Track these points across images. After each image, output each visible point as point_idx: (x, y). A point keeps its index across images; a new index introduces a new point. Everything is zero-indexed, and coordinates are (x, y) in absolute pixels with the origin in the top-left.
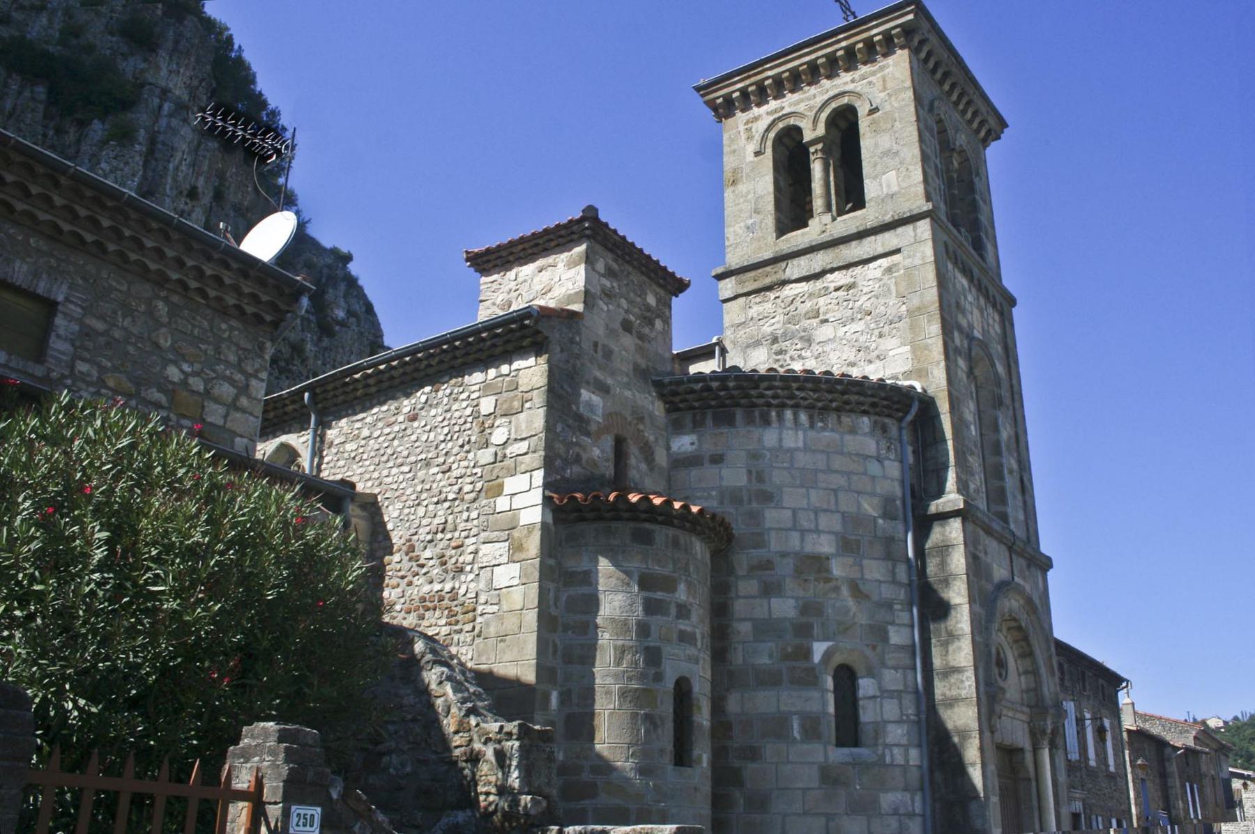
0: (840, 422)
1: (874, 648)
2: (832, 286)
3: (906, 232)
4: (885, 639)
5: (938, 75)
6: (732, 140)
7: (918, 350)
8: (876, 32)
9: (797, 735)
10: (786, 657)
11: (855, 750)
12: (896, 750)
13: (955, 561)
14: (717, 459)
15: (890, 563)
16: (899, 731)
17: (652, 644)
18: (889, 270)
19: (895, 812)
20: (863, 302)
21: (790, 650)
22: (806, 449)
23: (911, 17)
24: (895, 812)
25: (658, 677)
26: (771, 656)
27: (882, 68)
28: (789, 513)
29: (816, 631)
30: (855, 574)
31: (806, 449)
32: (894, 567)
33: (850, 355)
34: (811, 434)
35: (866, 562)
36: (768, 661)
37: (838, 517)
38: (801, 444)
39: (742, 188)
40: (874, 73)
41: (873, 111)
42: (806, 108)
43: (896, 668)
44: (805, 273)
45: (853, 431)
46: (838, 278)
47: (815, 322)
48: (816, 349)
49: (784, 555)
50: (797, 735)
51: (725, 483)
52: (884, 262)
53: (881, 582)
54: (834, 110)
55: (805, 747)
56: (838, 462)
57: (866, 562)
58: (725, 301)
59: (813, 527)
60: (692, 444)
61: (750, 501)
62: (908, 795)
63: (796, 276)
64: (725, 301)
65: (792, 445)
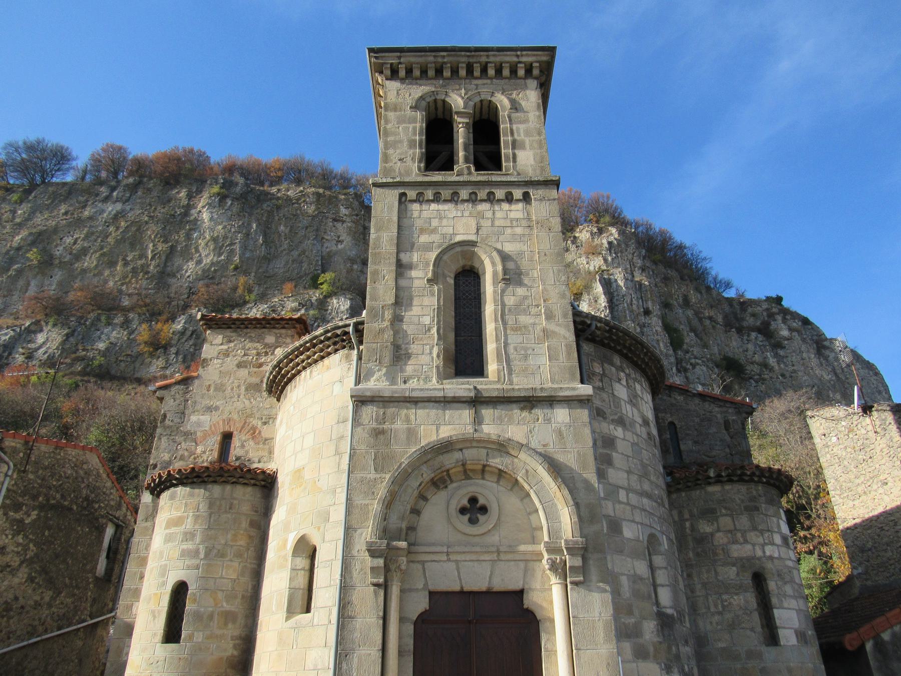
45: (328, 368)
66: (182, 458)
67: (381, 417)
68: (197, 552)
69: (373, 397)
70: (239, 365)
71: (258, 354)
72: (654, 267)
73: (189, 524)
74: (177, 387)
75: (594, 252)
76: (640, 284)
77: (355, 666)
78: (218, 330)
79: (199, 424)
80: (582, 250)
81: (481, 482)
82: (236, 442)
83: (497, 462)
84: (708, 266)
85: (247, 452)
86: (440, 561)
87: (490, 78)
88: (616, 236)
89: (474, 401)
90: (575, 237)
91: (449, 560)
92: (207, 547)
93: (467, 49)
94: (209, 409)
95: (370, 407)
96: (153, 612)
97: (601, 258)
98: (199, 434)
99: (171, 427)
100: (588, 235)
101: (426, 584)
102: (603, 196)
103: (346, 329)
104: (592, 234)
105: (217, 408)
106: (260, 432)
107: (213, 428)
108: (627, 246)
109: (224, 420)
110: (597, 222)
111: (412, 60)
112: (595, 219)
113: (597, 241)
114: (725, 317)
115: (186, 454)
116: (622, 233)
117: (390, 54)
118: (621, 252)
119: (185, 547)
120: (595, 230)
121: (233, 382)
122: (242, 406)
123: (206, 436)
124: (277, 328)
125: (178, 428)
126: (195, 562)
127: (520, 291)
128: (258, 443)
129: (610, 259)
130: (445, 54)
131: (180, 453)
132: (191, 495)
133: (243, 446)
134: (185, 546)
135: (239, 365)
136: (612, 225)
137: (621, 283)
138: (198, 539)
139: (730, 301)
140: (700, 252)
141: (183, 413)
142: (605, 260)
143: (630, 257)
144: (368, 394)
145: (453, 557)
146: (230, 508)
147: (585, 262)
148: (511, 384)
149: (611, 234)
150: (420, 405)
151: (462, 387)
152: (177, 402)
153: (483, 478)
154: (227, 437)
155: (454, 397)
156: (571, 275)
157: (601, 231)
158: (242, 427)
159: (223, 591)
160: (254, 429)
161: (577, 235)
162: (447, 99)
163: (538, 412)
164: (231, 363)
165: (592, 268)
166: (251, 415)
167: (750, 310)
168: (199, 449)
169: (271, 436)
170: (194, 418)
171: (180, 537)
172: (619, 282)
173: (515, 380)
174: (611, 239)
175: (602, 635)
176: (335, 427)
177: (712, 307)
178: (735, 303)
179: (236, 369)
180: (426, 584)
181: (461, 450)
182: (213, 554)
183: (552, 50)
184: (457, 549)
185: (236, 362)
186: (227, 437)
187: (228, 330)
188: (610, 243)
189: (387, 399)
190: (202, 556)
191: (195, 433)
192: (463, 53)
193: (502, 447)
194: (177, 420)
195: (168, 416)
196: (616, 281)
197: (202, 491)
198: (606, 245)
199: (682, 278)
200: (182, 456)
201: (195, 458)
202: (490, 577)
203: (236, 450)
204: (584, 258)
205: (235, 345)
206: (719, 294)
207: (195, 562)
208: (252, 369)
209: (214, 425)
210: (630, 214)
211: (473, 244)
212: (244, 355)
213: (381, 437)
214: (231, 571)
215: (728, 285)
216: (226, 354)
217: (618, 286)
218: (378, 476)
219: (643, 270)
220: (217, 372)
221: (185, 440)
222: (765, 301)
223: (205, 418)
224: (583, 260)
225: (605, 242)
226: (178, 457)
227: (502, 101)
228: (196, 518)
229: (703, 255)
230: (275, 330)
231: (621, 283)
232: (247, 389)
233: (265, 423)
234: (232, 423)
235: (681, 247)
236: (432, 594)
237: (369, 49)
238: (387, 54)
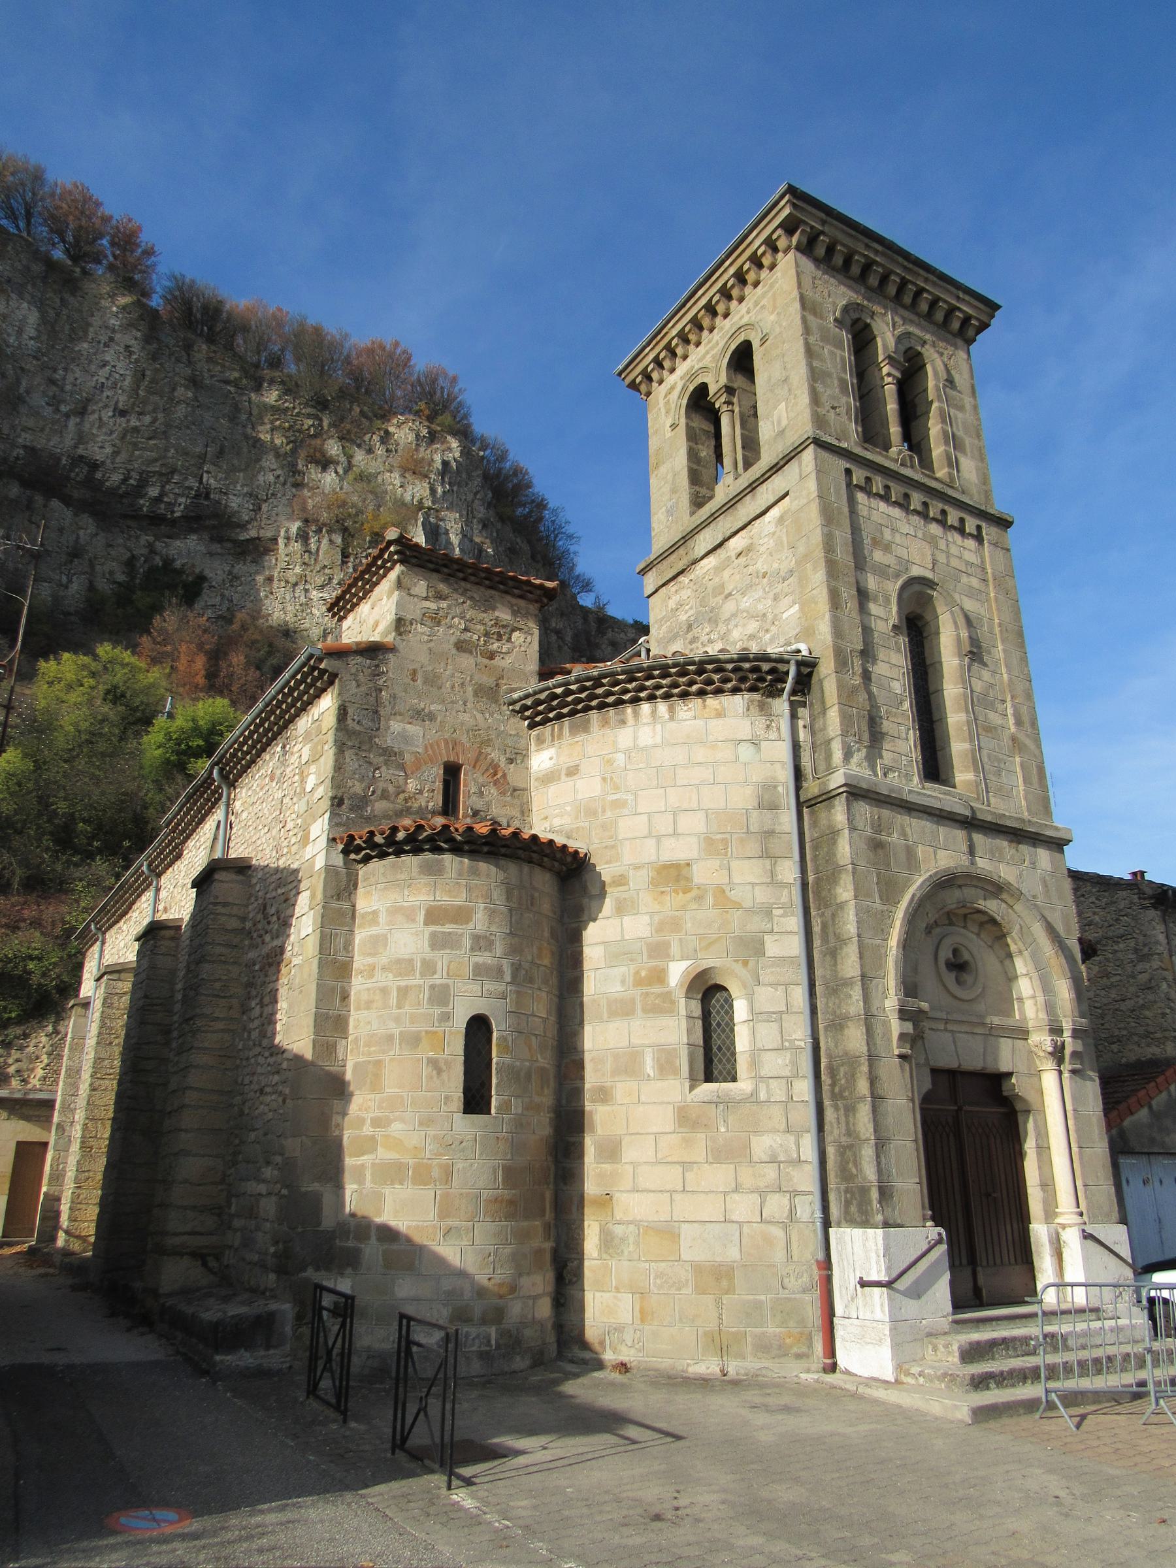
0: (705, 707)
1: (745, 963)
2: (733, 554)
3: (792, 469)
4: (760, 951)
5: (873, 281)
6: (656, 419)
7: (805, 605)
8: (757, 242)
9: (649, 1070)
10: (639, 982)
11: (58, 1105)
12: (774, 1084)
13: (840, 848)
14: (573, 771)
15: (768, 862)
16: (780, 1061)
17: (438, 982)
18: (781, 520)
19: (774, 1160)
20: (761, 565)
21: (643, 974)
22: (665, 743)
23: (787, 211)
24: (774, 1160)
25: (446, 1017)
26: (623, 982)
27: (772, 286)
28: (645, 818)
29: (675, 949)
30: (721, 878)
31: (665, 743)
32: (773, 865)
33: (753, 626)
34: (673, 725)
35: (735, 864)
36: (620, 989)
37: (701, 815)
38: (658, 740)
39: (663, 469)
40: (763, 295)
41: (764, 341)
42: (706, 360)
43: (774, 985)
44: (710, 547)
45: (720, 714)
46: (736, 543)
47: (719, 599)
48: (722, 628)
49: (637, 867)
50: (649, 1070)
51: (579, 797)
52: (774, 513)
53: (753, 885)
54: (734, 353)
55: (659, 1084)
56: (700, 754)
57: (735, 864)
58: (649, 597)
59: (671, 831)
60: (551, 759)
61: (604, 811)
62: (792, 1138)
63: (703, 553)
64: (649, 597)
65: (650, 742)
66: (385, 796)
67: (876, 823)
68: (500, 971)
69: (869, 791)
70: (461, 646)
71: (487, 634)
72: (499, 526)
73: (480, 922)
74: (359, 659)
75: (414, 469)
76: (481, 551)
77: (893, 1160)
78: (416, 569)
79: (405, 738)
80: (395, 460)
81: (962, 930)
82: (468, 782)
83: (992, 906)
84: (572, 548)
85: (489, 805)
86: (938, 1030)
87: (917, 314)
88: (457, 455)
89: (967, 823)
90: (387, 432)
91: (946, 1030)
92: (513, 964)
93: (906, 255)
94: (419, 715)
95: (861, 803)
96: (433, 1063)
97: (426, 485)
98: (407, 757)
99: (360, 733)
100: (411, 437)
101: (927, 1059)
102: (446, 375)
103: (782, 667)
104: (417, 435)
105: (431, 717)
106: (504, 776)
107: (430, 752)
108: (469, 477)
109: (446, 742)
110: (430, 419)
111: (840, 236)
112: (427, 412)
113: (423, 453)
114: (576, 636)
115: (391, 789)
116: (465, 452)
117: (814, 211)
118: (459, 485)
119: (480, 960)
120: (425, 432)
121: (453, 676)
122: (472, 722)
123: (418, 764)
124: (514, 596)
125: (371, 738)
126: (498, 987)
127: (986, 674)
128: (503, 793)
129: (440, 490)
130: (880, 248)
131: (381, 785)
132: (474, 872)
133: (481, 794)
134: (479, 958)
135: (461, 646)
136: (454, 434)
137: (455, 539)
138: (499, 949)
139: (585, 611)
140: (567, 522)
141: (376, 712)
142: (433, 491)
143: (470, 497)
144: (864, 786)
145: (950, 1027)
146: (532, 904)
147: (397, 482)
148: (989, 805)
149: (450, 449)
150: (914, 814)
151: (932, 794)
152: (363, 689)
153: (965, 927)
154: (452, 772)
155: (950, 812)
156: (370, 497)
157: (433, 438)
158: (477, 761)
159: (536, 1035)
160: (495, 767)
161: (392, 429)
162: (874, 325)
163: (1025, 849)
164: (446, 636)
165: (408, 498)
166: (488, 742)
167: (610, 634)
168: (412, 785)
169: (522, 786)
170: (396, 726)
171: (467, 943)
172: (452, 537)
173: (992, 800)
174: (449, 456)
175: (1097, 1132)
176: (755, 814)
177: (562, 615)
178: (591, 617)
179: (454, 651)
180: (927, 1059)
181: (960, 887)
182: (521, 977)
183: (994, 307)
184: (955, 1016)
185: (453, 639)
186: (452, 772)
187: (435, 575)
188: (445, 463)
189: (882, 798)
190: (508, 978)
191: (401, 753)
192: (900, 259)
193: (996, 889)
194: (367, 723)
195: (350, 711)
196: (447, 532)
197: (493, 869)
198: (438, 464)
199: (533, 557)
200: (384, 791)
201: (406, 800)
202: (984, 1055)
203: (467, 799)
204: (396, 475)
205: (449, 607)
206: (574, 597)
207: (498, 987)
208: (480, 659)
209: (431, 745)
210: (481, 426)
211: (931, 584)
212: (466, 630)
213: (880, 851)
214: (541, 1005)
215: (587, 586)
216: (436, 619)
217: (449, 542)
218: (885, 908)
219: (485, 526)
220: (425, 647)
221: (386, 764)
222: (632, 626)
223: (414, 730)
224: (395, 479)
225: (438, 458)
226: (379, 792)
227: (929, 353)
228: (492, 913)
229: (570, 529)
230: (509, 598)
231: (455, 539)
232: (476, 694)
233: (511, 761)
234: (459, 749)
235: (541, 505)
236: (935, 1072)
237: (790, 186)
238: (809, 208)
